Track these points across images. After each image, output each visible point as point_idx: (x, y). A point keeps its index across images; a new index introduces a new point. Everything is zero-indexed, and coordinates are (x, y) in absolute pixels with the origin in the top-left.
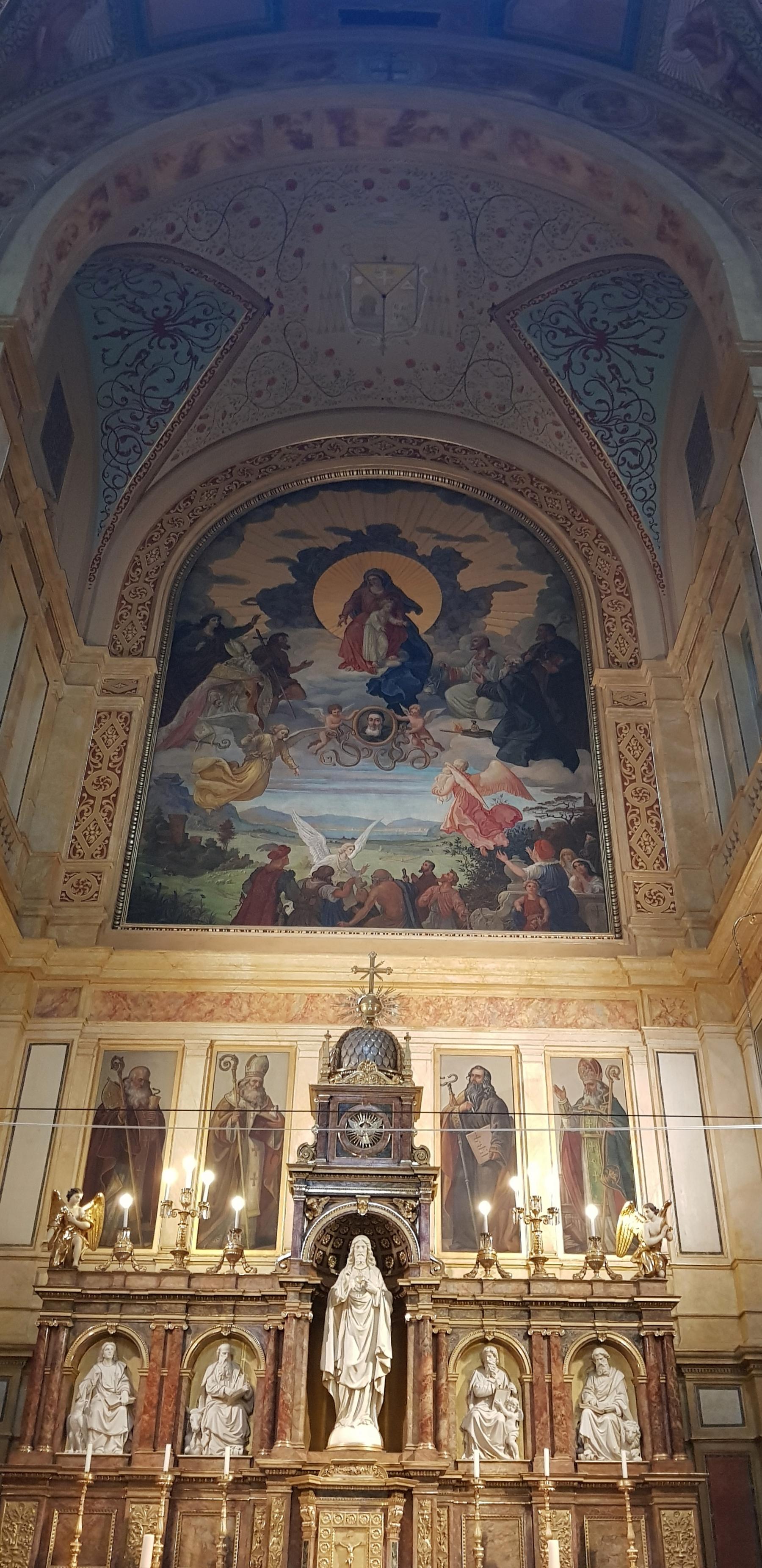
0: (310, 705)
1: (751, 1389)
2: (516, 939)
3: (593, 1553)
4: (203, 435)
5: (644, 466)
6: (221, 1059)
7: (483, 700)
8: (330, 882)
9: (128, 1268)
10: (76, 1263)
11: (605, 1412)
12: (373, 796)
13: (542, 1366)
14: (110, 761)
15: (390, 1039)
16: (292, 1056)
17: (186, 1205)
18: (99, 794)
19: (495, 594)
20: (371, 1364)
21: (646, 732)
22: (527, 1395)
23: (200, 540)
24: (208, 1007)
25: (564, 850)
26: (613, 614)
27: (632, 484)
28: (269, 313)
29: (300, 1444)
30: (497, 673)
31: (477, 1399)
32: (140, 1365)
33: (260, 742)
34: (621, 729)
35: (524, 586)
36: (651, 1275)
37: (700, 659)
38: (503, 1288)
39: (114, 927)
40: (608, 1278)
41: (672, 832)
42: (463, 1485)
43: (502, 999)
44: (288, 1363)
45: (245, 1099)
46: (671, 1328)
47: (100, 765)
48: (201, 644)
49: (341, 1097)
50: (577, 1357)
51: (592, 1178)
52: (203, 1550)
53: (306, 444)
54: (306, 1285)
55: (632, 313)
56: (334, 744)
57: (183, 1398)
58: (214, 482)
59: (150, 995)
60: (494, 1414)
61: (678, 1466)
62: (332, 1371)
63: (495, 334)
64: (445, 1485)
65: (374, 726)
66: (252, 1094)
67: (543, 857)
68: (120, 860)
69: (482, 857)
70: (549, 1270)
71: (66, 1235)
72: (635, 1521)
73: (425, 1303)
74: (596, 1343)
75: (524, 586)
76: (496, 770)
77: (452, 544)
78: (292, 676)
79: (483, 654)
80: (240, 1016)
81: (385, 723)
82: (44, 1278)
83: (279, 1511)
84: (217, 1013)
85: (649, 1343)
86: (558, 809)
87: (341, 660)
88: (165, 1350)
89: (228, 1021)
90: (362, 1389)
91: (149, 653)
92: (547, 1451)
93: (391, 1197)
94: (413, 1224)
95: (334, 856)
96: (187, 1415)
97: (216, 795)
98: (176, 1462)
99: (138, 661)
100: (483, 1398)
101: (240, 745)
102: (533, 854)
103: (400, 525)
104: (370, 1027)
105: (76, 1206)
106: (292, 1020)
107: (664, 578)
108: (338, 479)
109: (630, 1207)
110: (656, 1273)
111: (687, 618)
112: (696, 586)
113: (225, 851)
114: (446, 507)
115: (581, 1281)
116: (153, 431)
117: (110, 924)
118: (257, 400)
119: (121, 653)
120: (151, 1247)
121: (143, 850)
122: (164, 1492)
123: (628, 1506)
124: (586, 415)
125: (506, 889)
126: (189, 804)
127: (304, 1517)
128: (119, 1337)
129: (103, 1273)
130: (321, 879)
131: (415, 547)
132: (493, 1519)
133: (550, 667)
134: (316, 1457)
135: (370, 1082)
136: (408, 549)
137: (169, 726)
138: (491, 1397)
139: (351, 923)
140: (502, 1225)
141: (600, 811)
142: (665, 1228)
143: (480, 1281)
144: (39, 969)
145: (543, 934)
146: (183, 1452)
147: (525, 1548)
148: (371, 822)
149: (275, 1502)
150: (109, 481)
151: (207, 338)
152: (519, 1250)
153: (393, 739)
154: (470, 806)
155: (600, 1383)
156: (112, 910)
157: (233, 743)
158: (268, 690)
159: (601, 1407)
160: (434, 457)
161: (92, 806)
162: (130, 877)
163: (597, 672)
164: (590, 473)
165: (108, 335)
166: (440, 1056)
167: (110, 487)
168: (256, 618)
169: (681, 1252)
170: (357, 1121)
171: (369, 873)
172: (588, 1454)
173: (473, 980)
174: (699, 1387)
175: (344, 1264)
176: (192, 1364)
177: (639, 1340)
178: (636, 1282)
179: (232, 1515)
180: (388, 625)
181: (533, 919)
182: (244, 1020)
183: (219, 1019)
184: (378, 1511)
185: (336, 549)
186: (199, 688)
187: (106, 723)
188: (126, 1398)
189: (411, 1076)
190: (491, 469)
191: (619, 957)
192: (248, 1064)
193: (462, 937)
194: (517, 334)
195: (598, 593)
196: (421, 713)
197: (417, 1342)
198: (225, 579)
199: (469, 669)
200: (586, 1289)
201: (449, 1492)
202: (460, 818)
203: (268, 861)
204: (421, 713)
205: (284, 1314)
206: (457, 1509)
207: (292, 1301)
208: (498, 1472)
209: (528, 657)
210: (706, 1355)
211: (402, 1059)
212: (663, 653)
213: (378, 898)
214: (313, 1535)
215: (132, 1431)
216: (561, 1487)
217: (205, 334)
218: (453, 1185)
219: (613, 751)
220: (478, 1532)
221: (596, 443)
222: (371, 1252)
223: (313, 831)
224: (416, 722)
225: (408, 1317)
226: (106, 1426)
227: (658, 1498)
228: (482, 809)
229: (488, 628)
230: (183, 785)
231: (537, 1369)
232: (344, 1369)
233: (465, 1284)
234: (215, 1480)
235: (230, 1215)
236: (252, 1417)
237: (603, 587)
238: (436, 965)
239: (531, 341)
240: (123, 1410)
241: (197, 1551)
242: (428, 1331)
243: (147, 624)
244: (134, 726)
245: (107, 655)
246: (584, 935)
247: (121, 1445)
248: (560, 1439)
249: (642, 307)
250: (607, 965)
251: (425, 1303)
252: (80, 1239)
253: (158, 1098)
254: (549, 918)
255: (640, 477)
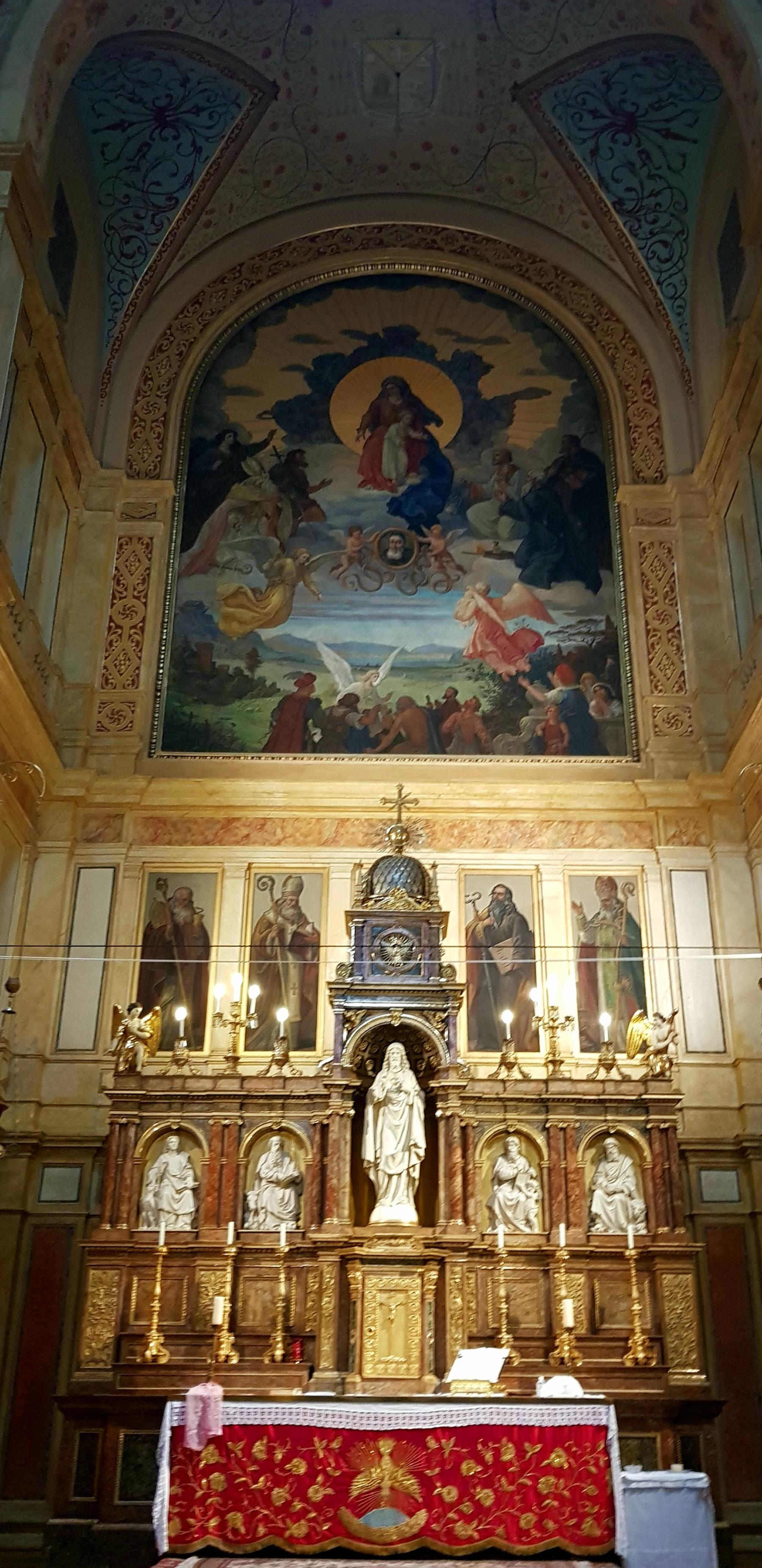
0: (331, 528)
1: (748, 1170)
2: (537, 764)
3: (602, 1310)
4: (210, 230)
5: (675, 259)
6: (260, 880)
7: (506, 520)
8: (356, 710)
9: (186, 1070)
10: (139, 1069)
11: (615, 1193)
12: (395, 622)
13: (559, 1153)
14: (135, 589)
15: (416, 865)
16: (325, 877)
17: (235, 1016)
18: (126, 623)
19: (517, 402)
20: (407, 1154)
21: (670, 551)
22: (545, 1178)
23: (211, 348)
24: (245, 831)
25: (585, 675)
26: (639, 423)
27: (662, 280)
28: (276, 98)
29: (347, 1221)
30: (519, 490)
31: (501, 1182)
32: (203, 1155)
33: (282, 568)
34: (644, 548)
35: (548, 393)
36: (658, 1075)
37: (726, 478)
38: (523, 1087)
39: (150, 756)
40: (618, 1078)
41: (692, 654)
42: (489, 1254)
43: (523, 822)
44: (333, 1153)
45: (283, 917)
46: (674, 1121)
47: (125, 594)
48: (218, 463)
49: (374, 921)
50: (590, 1146)
51: (606, 986)
52: (265, 1308)
53: (318, 236)
54: (347, 1087)
55: (664, 95)
56: (356, 569)
57: (241, 1183)
58: (222, 282)
59: (189, 820)
60: (515, 1194)
61: (679, 1238)
62: (372, 1160)
63: (518, 115)
64: (473, 1253)
65: (396, 549)
66: (289, 912)
67: (565, 681)
68: (151, 689)
69: (505, 683)
70: (565, 1070)
71: (129, 1044)
72: (640, 1283)
73: (454, 1102)
74: (606, 1134)
75: (548, 393)
76: (517, 594)
77: (473, 347)
78: (311, 496)
79: (505, 468)
80: (274, 839)
81: (407, 546)
82: (109, 1080)
83: (330, 1278)
84: (254, 836)
85: (656, 1135)
86: (579, 633)
87: (361, 478)
88: (223, 1142)
89: (264, 844)
90: (400, 1175)
91: (166, 474)
92: (562, 1226)
93: (421, 1010)
94: (442, 1033)
95: (358, 684)
96: (245, 1197)
97: (241, 622)
98: (237, 1236)
99: (156, 484)
100: (507, 1181)
101: (262, 571)
102: (554, 678)
103: (418, 327)
104: (399, 855)
105: (136, 1019)
106: (324, 844)
107: (692, 384)
108: (352, 275)
109: (641, 1015)
110: (662, 1073)
111: (713, 436)
112: (727, 395)
113: (251, 680)
114: (466, 304)
115: (593, 1081)
116: (158, 231)
117: (146, 754)
118: (266, 191)
119: (138, 474)
120: (201, 1049)
121: (173, 679)
122: (230, 1261)
123: (633, 1272)
124: (614, 204)
125: (527, 715)
126: (215, 632)
127: (352, 1281)
128: (181, 1132)
129: (163, 1077)
130: (347, 707)
131: (434, 351)
132: (515, 1281)
133: (573, 482)
134: (360, 1231)
135: (400, 907)
136: (427, 354)
137: (190, 551)
138: (513, 1180)
139: (378, 749)
140: (522, 1028)
141: (622, 634)
142: (672, 1034)
143: (503, 1081)
144: (82, 798)
145: (564, 759)
146: (242, 1227)
147: (543, 1305)
148: (394, 648)
149: (326, 1269)
150: (115, 285)
151: (210, 128)
152: (537, 1050)
153: (415, 563)
154: (492, 630)
155: (609, 1167)
156: (147, 740)
157: (255, 569)
158: (288, 511)
159: (612, 1187)
160: (454, 248)
161: (120, 635)
162: (161, 706)
163: (622, 488)
164: (618, 267)
165: (109, 128)
166: (466, 876)
167: (115, 293)
168: (272, 433)
169: (688, 1052)
170: (390, 942)
171: (394, 700)
172: (598, 1228)
173: (496, 804)
174: (702, 1169)
175: (381, 1069)
176: (247, 1154)
177: (645, 1132)
178: (644, 1081)
179: (288, 1279)
180: (409, 440)
181: (554, 744)
182: (278, 843)
183: (254, 843)
184: (416, 1276)
185: (352, 355)
186: (218, 510)
187: (128, 549)
188: (190, 1183)
189: (438, 901)
190: (513, 261)
191: (637, 781)
192: (285, 884)
193: (485, 762)
194: (541, 115)
195: (625, 401)
196: (443, 534)
197: (448, 1134)
198: (239, 391)
199: (491, 485)
200: (599, 1087)
201: (477, 1259)
202: (483, 644)
203: (295, 689)
204: (443, 534)
205: (329, 1112)
206: (484, 1273)
207: (335, 1101)
208: (520, 1244)
209: (552, 472)
210: (708, 1142)
211: (430, 885)
212: (689, 465)
213: (402, 725)
214: (360, 1296)
215: (197, 1211)
216: (574, 1255)
217: (210, 123)
218: (478, 993)
219: (636, 572)
220: (502, 1292)
221: (624, 235)
222: (405, 1057)
223: (338, 657)
224: (437, 544)
225: (439, 1113)
226: (176, 1206)
227: (660, 1265)
228: (504, 633)
229: (510, 441)
230: (207, 613)
231: (555, 1157)
232: (383, 1158)
233: (490, 1084)
234: (273, 1251)
235: (274, 1024)
236: (302, 1197)
237: (629, 393)
238: (461, 791)
239: (555, 122)
240: (189, 1193)
241: (259, 1308)
242: (457, 1124)
243: (162, 442)
244: (156, 552)
245: (125, 479)
246: (604, 759)
247: (189, 1221)
248: (574, 1215)
249: (674, 89)
250: (624, 788)
251: (454, 1102)
252: (141, 1048)
253: (202, 916)
254: (569, 742)
255: (671, 272)
